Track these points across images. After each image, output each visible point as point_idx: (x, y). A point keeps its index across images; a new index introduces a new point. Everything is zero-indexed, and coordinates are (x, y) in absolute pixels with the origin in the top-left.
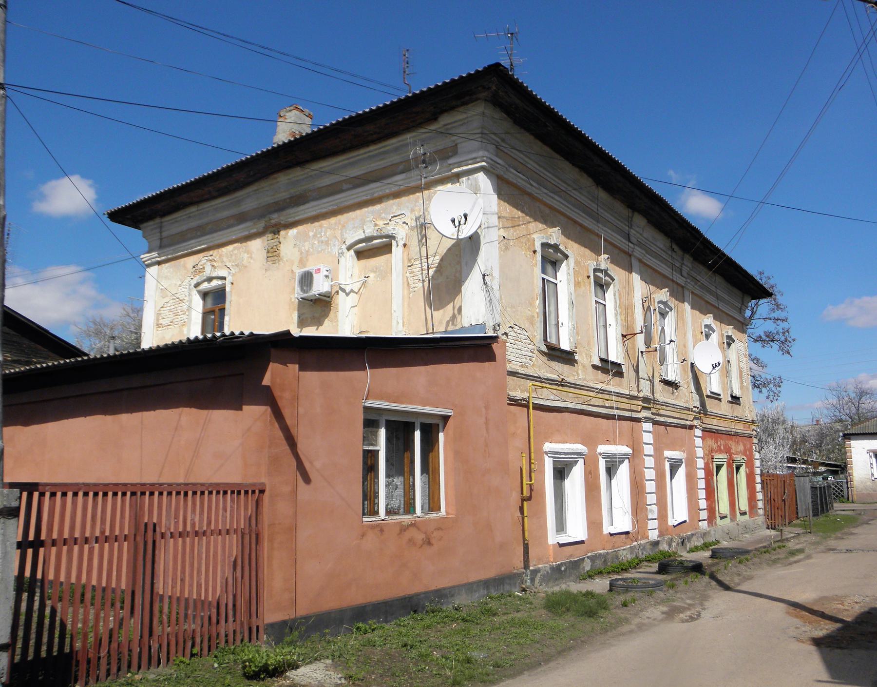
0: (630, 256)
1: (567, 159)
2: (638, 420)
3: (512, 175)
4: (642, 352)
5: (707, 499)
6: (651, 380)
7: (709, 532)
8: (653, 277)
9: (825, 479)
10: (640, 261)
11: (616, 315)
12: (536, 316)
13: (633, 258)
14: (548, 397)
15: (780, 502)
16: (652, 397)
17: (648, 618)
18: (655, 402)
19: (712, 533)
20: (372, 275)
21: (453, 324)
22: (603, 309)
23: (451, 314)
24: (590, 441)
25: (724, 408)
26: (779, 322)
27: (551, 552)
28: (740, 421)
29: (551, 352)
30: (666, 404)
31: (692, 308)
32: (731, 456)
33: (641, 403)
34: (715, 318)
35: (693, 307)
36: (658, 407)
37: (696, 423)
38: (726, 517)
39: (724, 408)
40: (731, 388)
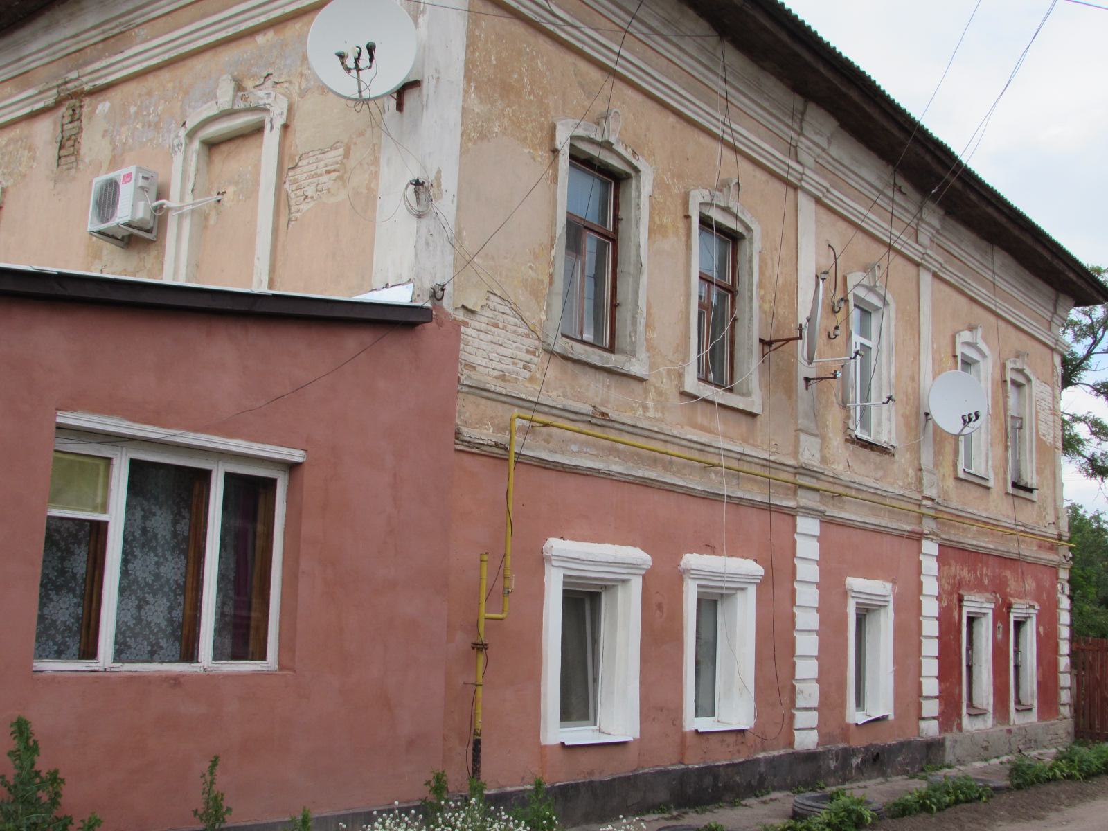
2: (791, 514)
5: (941, 677)
20: (231, 190)
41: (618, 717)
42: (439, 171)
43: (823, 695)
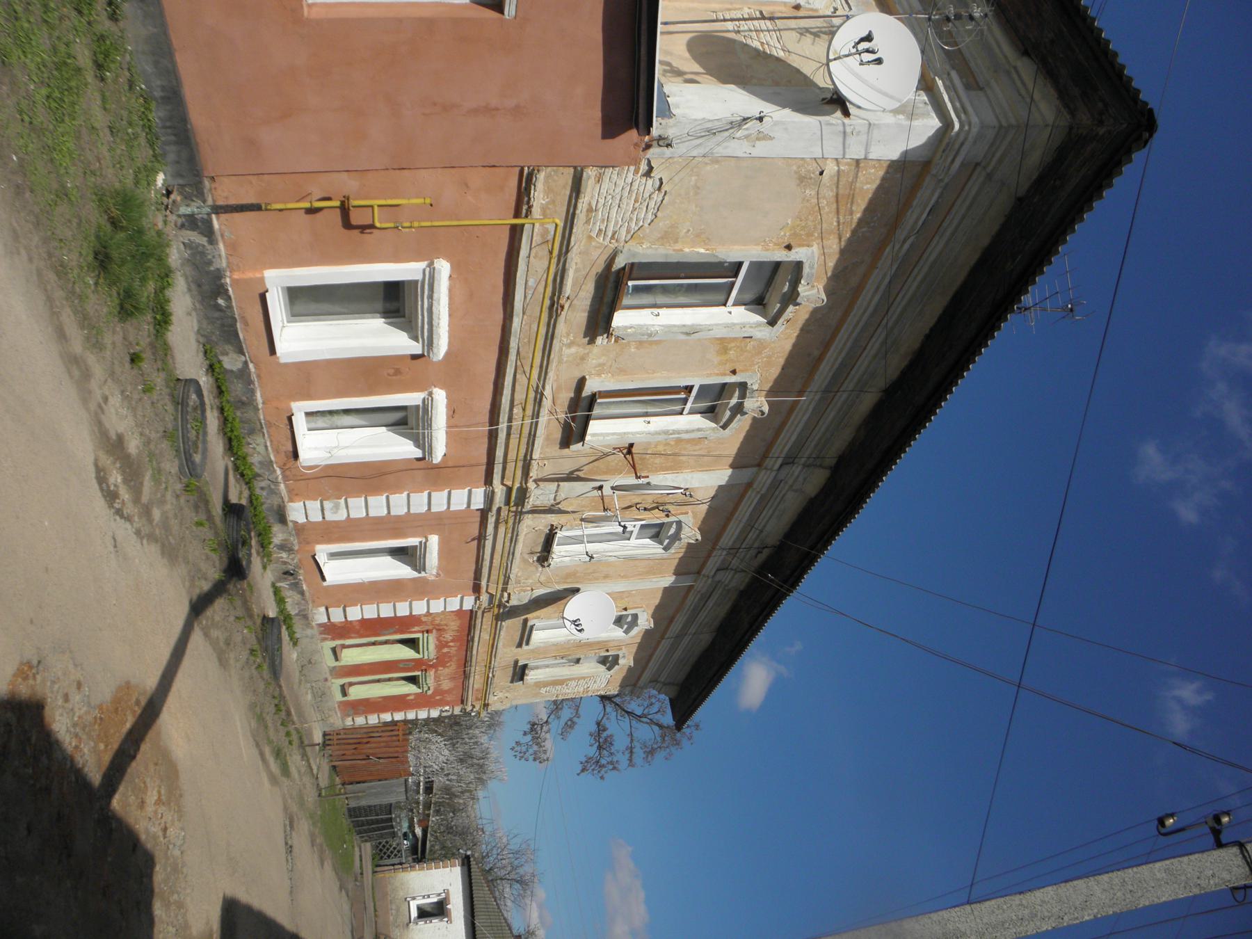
0: (759, 465)
1: (940, 320)
2: (488, 480)
3: (928, 194)
4: (600, 488)
6: (551, 510)
7: (309, 625)
8: (723, 507)
9: (405, 835)
10: (749, 485)
11: (666, 432)
12: (677, 247)
13: (755, 469)
14: (533, 270)
15: (362, 756)
16: (528, 507)
17: (106, 399)
18: (519, 515)
19: (309, 632)
21: (665, 71)
22: (673, 415)
23: (685, 69)
24: (453, 373)
25: (507, 653)
26: (627, 756)
27: (250, 275)
28: (488, 682)
29: (612, 279)
30: (514, 539)
31: (666, 590)
32: (431, 666)
33: (517, 485)
34: (648, 633)
35: (667, 591)
36: (511, 522)
37: (484, 598)
38: (337, 659)
39: (507, 653)
40: (537, 668)
41: (298, 340)
42: (771, 138)
43: (336, 524)
